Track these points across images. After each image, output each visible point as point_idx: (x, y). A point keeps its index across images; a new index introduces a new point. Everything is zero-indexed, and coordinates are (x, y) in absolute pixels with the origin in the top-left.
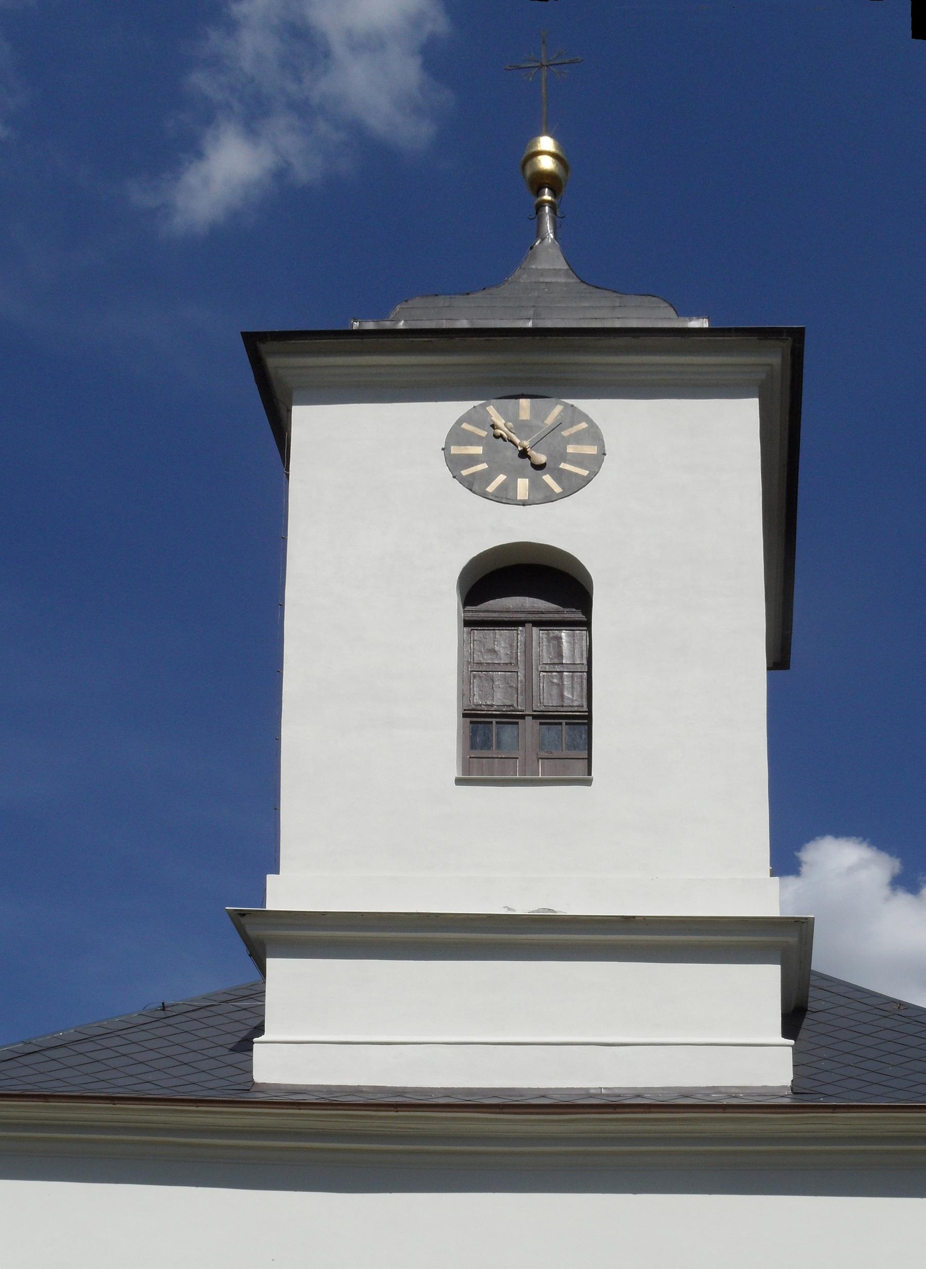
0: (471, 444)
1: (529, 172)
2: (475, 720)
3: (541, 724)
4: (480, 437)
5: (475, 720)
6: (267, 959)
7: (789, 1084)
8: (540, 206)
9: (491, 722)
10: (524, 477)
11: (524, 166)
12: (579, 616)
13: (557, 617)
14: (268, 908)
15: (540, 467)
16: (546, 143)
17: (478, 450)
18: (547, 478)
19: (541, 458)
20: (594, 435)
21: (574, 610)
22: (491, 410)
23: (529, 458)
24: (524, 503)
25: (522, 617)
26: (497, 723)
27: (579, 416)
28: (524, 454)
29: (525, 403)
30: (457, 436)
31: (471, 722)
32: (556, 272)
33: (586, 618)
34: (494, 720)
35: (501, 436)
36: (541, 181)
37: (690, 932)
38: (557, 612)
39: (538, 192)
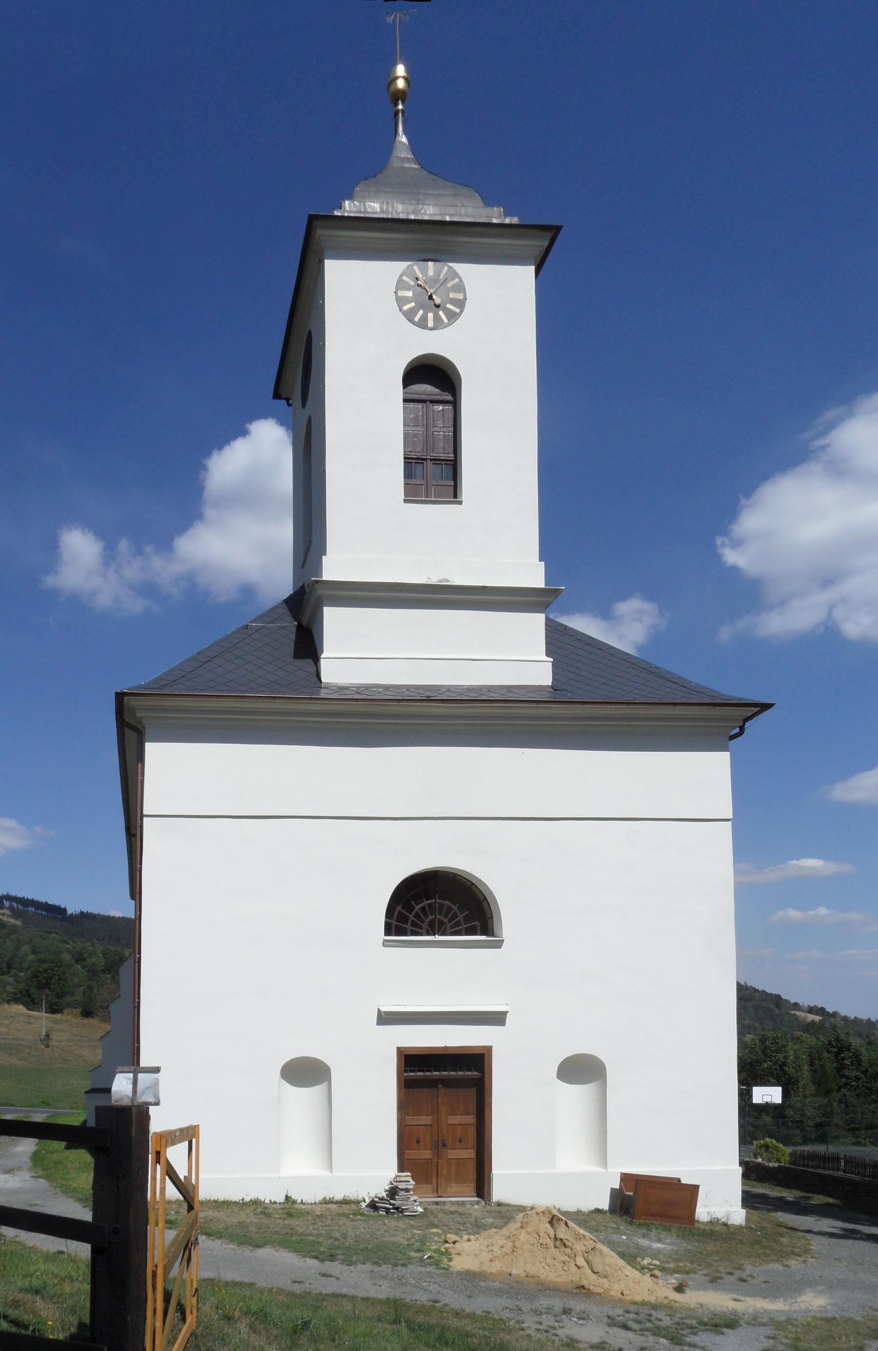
0: (450, 310)
1: (392, 88)
2: (447, 462)
3: (433, 464)
4: (451, 304)
5: (447, 462)
6: (325, 608)
7: (550, 684)
8: (396, 113)
9: (412, 462)
10: (431, 312)
11: (389, 86)
12: (449, 398)
13: (440, 398)
14: (324, 579)
15: (438, 306)
16: (401, 70)
17: (410, 294)
18: (441, 313)
19: (437, 300)
20: (460, 288)
21: (447, 394)
22: (415, 267)
23: (433, 300)
24: (431, 329)
25: (424, 397)
26: (415, 463)
27: (455, 275)
28: (431, 297)
29: (430, 264)
30: (401, 284)
31: (433, 464)
32: (407, 160)
33: (452, 396)
34: (413, 461)
35: (421, 286)
36: (399, 96)
37: (503, 595)
38: (441, 395)
39: (396, 105)
